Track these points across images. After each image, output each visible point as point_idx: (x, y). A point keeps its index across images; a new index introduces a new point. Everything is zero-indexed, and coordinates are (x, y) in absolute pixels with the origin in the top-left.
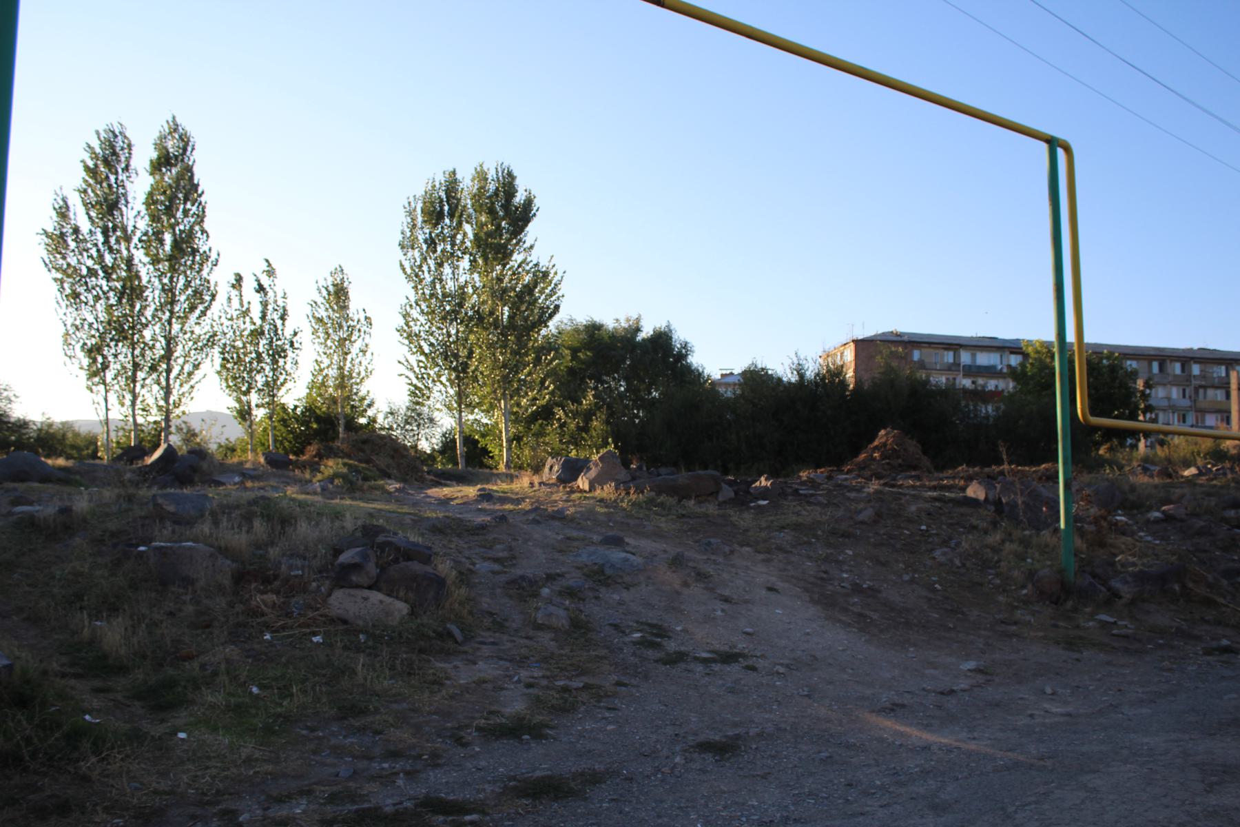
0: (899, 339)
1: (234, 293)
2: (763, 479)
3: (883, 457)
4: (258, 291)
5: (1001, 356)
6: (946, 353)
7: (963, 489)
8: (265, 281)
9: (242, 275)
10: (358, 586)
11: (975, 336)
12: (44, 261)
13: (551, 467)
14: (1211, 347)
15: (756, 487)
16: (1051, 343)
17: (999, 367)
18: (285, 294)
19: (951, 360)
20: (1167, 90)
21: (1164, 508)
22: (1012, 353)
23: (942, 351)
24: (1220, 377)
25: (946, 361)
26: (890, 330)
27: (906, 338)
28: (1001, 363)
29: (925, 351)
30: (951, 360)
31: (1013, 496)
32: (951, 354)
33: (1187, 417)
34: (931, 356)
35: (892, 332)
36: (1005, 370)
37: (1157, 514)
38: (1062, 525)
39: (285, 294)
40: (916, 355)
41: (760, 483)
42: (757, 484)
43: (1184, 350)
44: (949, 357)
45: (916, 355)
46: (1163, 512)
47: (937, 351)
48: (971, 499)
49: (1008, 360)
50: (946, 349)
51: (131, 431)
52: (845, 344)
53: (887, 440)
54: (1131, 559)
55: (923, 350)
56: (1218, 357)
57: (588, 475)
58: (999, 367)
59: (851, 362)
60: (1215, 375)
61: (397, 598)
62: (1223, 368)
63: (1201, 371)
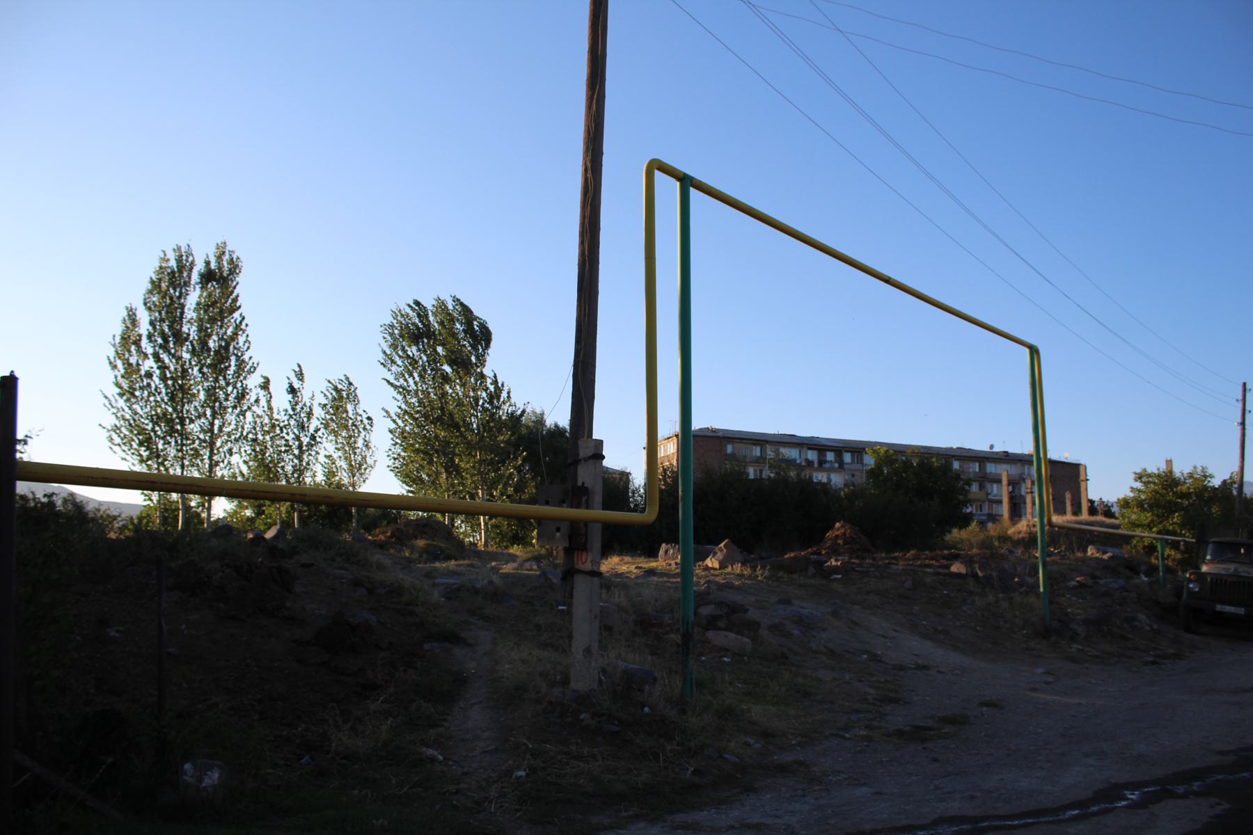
0: (714, 434)
1: (262, 393)
2: (833, 560)
3: (846, 543)
4: (289, 393)
5: (800, 451)
6: (754, 447)
7: (948, 567)
8: (296, 385)
9: (270, 378)
10: (720, 629)
11: (777, 433)
12: (388, 382)
13: (666, 552)
14: (967, 447)
15: (828, 566)
16: (1032, 456)
17: (798, 462)
18: (313, 396)
19: (758, 454)
20: (710, 35)
21: (1078, 579)
22: (809, 449)
23: (751, 446)
24: (974, 472)
25: (754, 454)
26: (706, 427)
27: (720, 434)
28: (800, 457)
29: (738, 445)
30: (758, 454)
31: (989, 572)
32: (758, 448)
33: (983, 507)
34: (743, 450)
35: (708, 428)
36: (803, 464)
37: (1074, 583)
38: (1041, 590)
39: (313, 396)
40: (729, 449)
41: (831, 563)
42: (829, 563)
43: (946, 449)
44: (757, 451)
45: (729, 449)
46: (1078, 581)
47: (747, 446)
48: (505, 519)
49: (806, 455)
50: (754, 444)
51: (160, 495)
52: (668, 438)
53: (846, 530)
54: (1077, 611)
55: (735, 444)
56: (974, 455)
57: (716, 557)
58: (798, 462)
59: (673, 454)
60: (971, 470)
61: (569, 613)
62: (977, 464)
63: (960, 466)
